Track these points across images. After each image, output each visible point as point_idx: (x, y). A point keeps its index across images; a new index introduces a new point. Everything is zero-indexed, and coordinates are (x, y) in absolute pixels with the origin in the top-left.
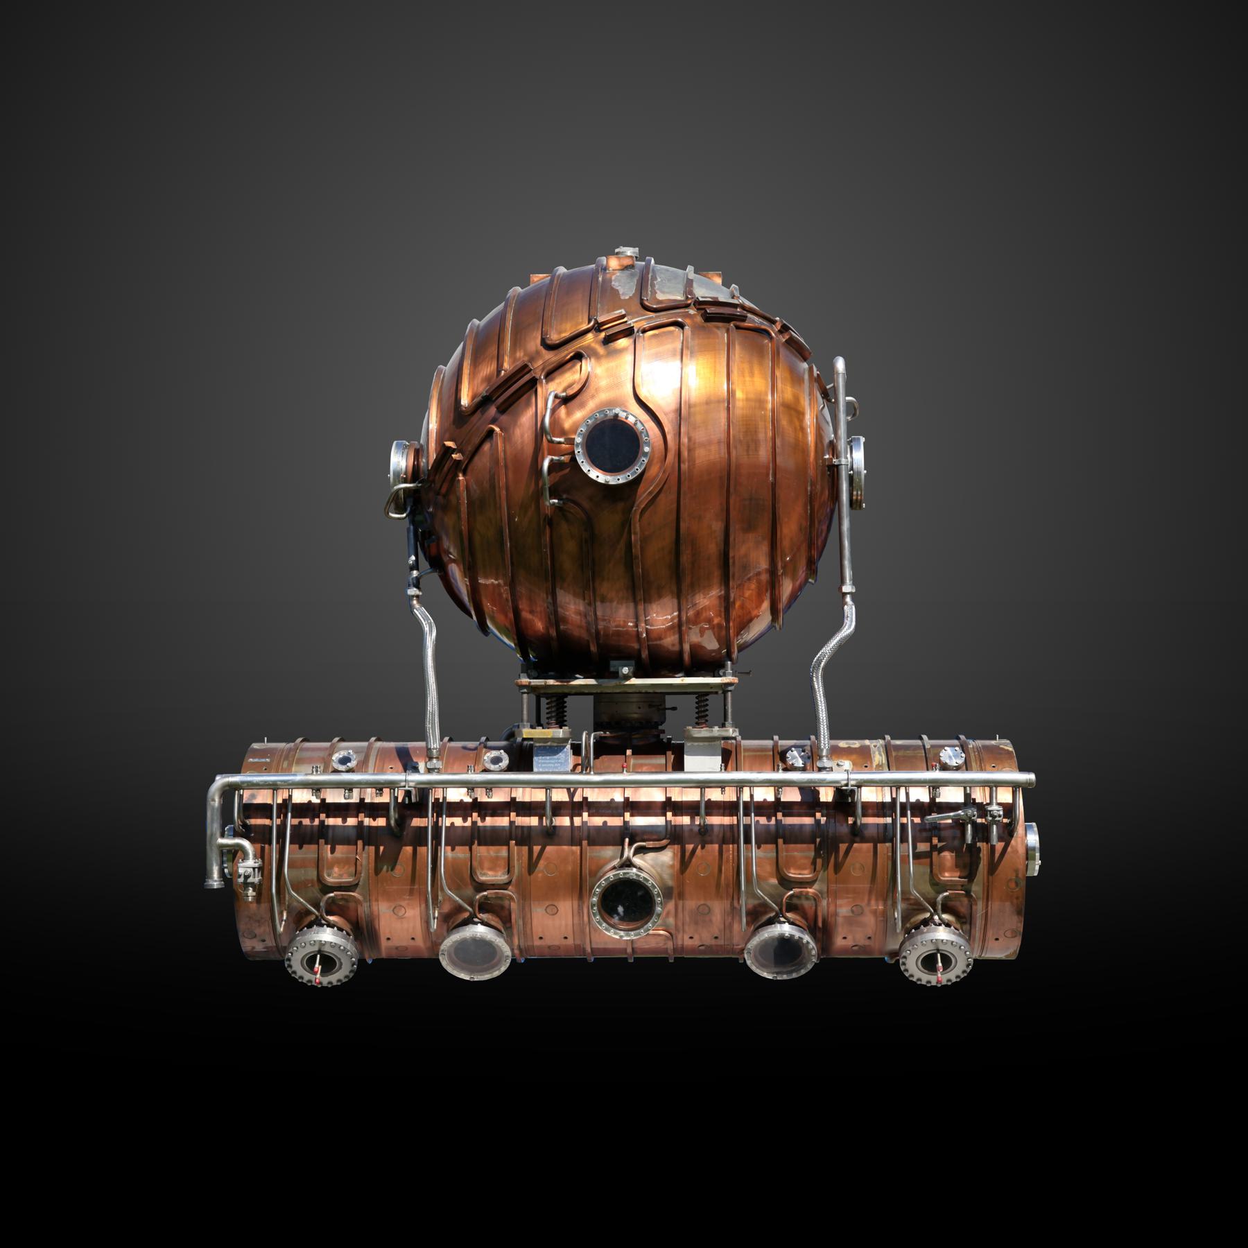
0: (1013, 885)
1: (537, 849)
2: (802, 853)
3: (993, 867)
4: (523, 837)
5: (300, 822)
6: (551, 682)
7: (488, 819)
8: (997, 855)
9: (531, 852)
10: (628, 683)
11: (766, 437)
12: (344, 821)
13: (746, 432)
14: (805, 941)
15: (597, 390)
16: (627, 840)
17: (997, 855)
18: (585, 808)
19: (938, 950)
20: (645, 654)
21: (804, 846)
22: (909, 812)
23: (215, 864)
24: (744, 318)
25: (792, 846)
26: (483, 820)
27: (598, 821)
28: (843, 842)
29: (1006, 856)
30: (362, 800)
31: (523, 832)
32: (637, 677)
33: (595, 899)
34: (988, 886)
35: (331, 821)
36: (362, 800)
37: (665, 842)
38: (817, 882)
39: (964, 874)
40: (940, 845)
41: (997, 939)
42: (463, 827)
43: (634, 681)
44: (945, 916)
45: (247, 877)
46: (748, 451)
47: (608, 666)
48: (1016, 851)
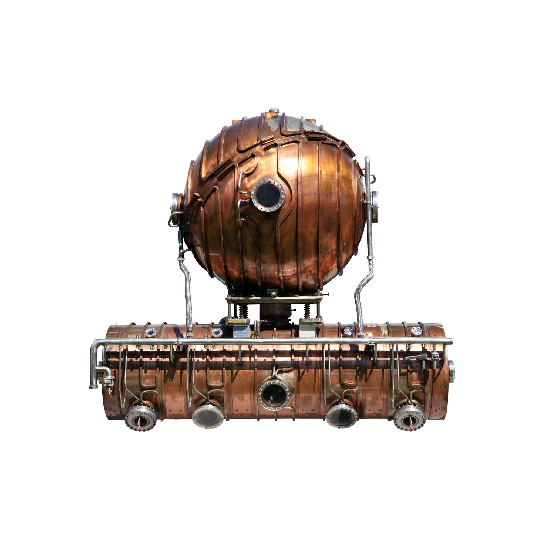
0: (443, 387)
1: (235, 371)
2: (351, 373)
3: (434, 379)
4: (229, 366)
5: (131, 360)
6: (241, 298)
7: (213, 358)
8: (436, 374)
9: (232, 373)
10: (275, 299)
11: (335, 191)
12: (151, 359)
13: (327, 189)
14: (352, 412)
15: (261, 171)
16: (274, 367)
17: (436, 374)
18: (256, 353)
19: (410, 416)
20: (282, 286)
21: (352, 370)
22: (398, 355)
23: (94, 378)
24: (325, 139)
25: (347, 370)
26: (211, 359)
27: (261, 359)
28: (369, 368)
29: (440, 374)
30: (158, 350)
31: (229, 364)
32: (279, 296)
33: (260, 393)
34: (432, 388)
35: (145, 359)
36: (158, 350)
37: (291, 368)
38: (358, 386)
39: (422, 382)
40: (411, 370)
41: (436, 411)
42: (203, 362)
43: (277, 298)
44: (413, 401)
45: (108, 384)
46: (327, 197)
47: (266, 291)
48: (444, 372)
